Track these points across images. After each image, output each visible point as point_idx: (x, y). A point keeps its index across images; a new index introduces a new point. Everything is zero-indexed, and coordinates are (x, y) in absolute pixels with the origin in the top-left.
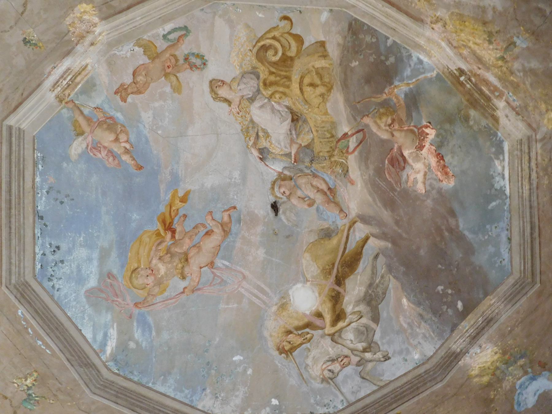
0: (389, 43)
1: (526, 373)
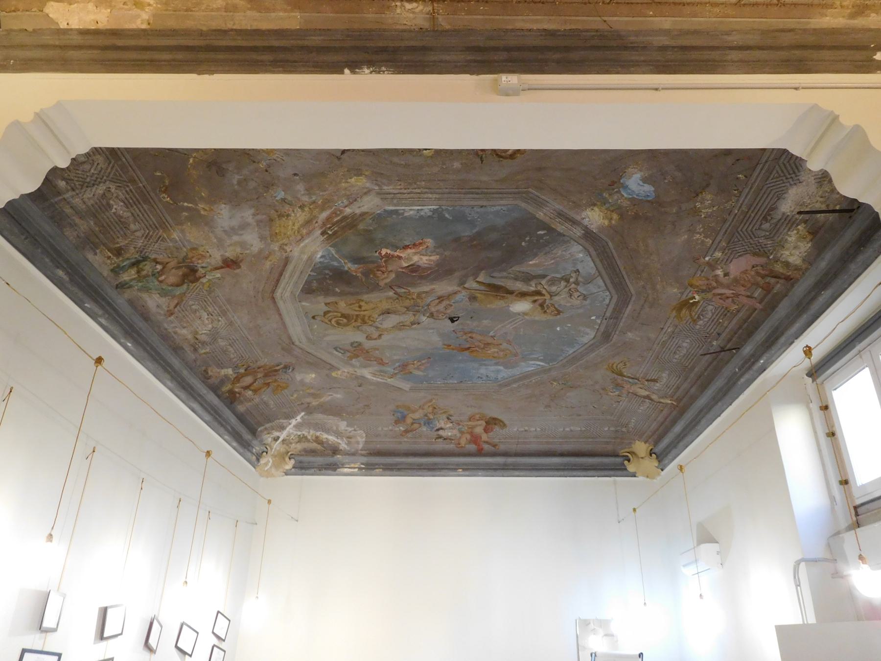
1: (619, 192)
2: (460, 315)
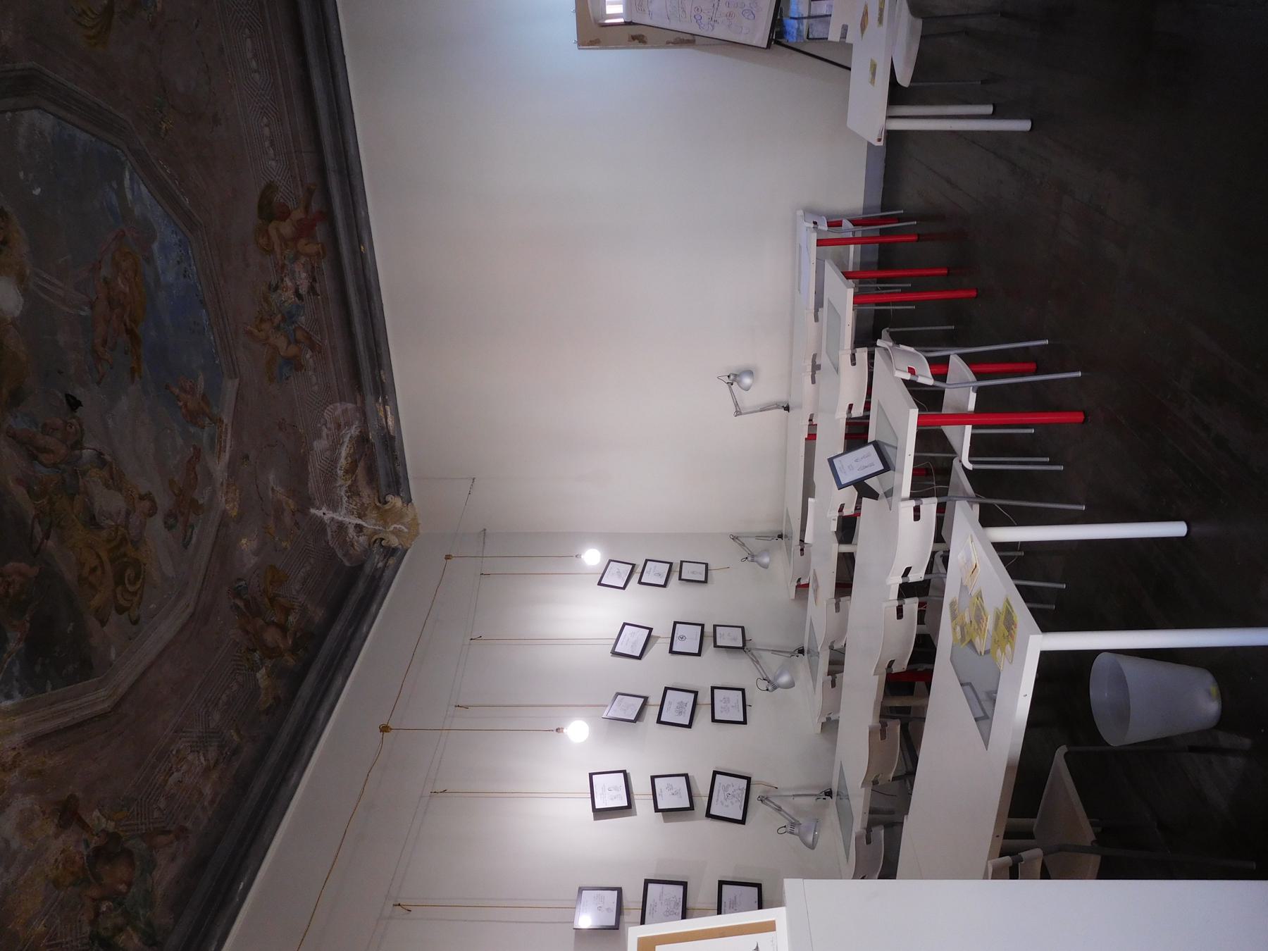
0: (49, 687)
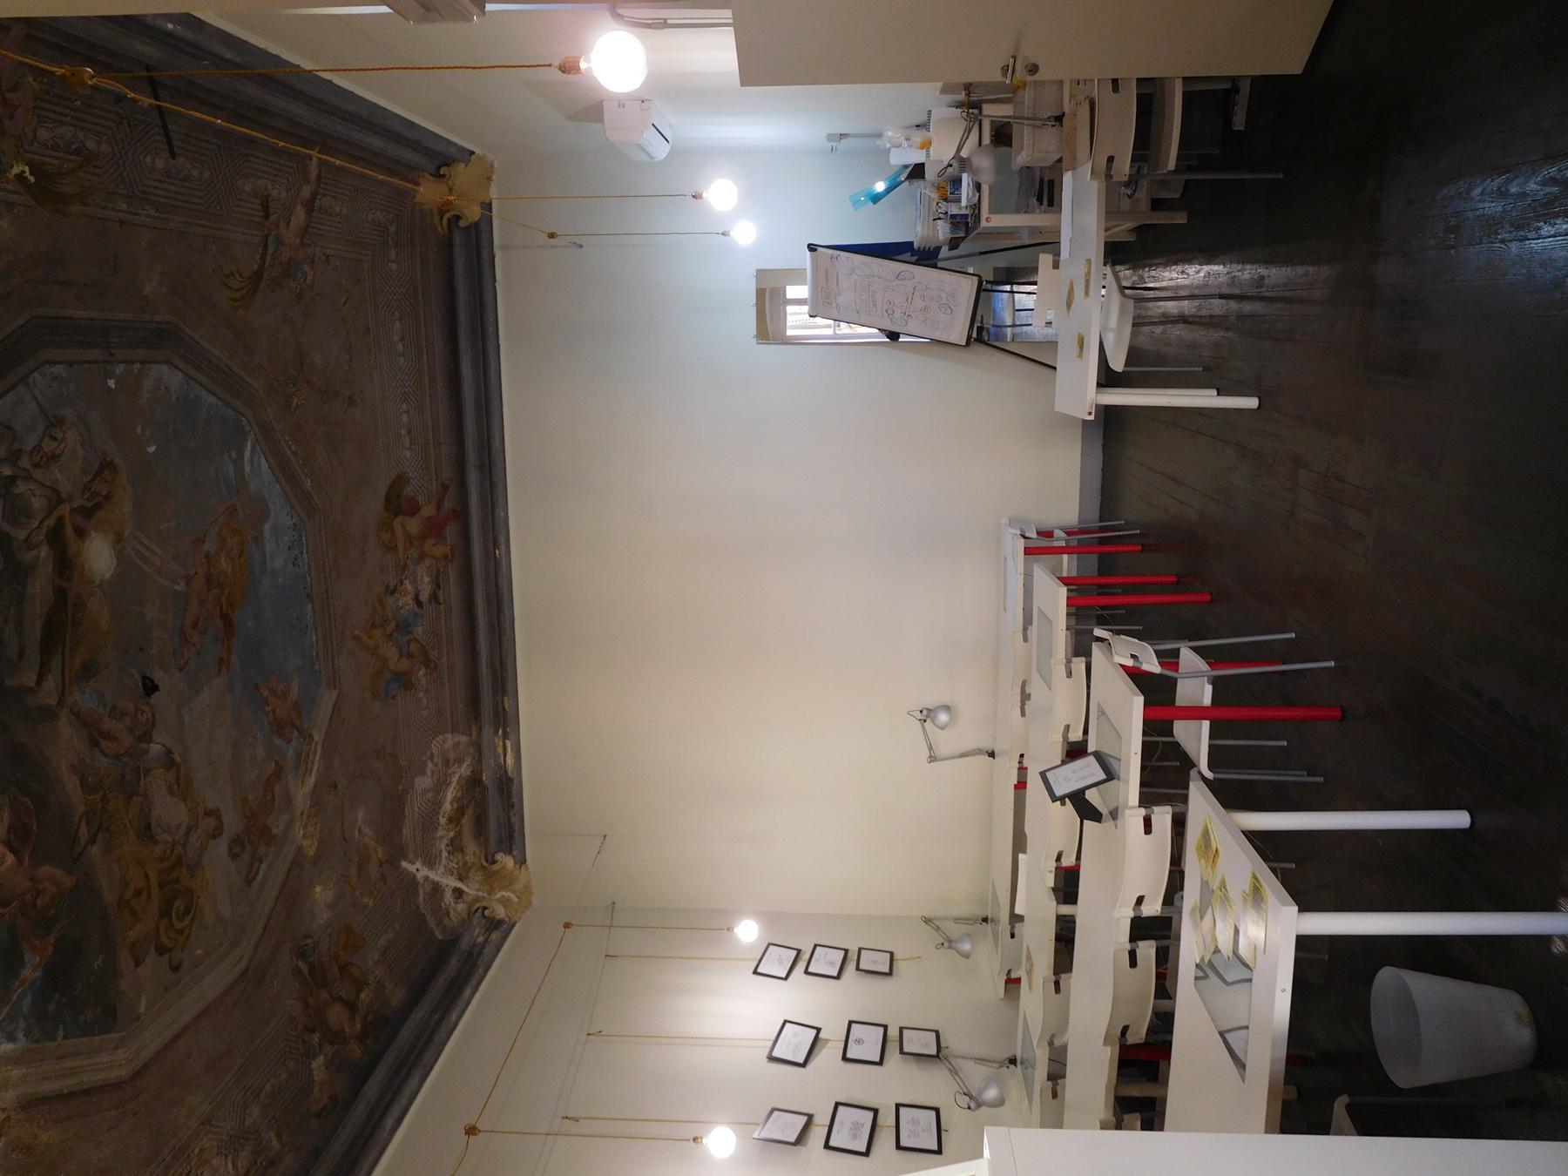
0: (61, 1033)
2: (138, 677)
